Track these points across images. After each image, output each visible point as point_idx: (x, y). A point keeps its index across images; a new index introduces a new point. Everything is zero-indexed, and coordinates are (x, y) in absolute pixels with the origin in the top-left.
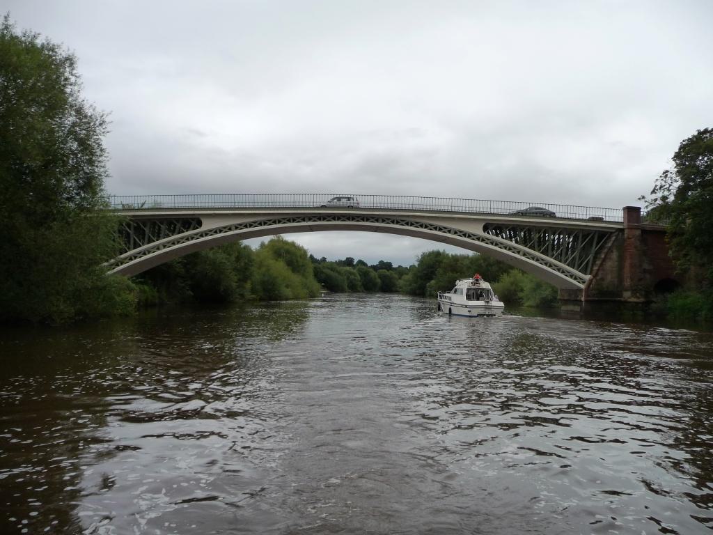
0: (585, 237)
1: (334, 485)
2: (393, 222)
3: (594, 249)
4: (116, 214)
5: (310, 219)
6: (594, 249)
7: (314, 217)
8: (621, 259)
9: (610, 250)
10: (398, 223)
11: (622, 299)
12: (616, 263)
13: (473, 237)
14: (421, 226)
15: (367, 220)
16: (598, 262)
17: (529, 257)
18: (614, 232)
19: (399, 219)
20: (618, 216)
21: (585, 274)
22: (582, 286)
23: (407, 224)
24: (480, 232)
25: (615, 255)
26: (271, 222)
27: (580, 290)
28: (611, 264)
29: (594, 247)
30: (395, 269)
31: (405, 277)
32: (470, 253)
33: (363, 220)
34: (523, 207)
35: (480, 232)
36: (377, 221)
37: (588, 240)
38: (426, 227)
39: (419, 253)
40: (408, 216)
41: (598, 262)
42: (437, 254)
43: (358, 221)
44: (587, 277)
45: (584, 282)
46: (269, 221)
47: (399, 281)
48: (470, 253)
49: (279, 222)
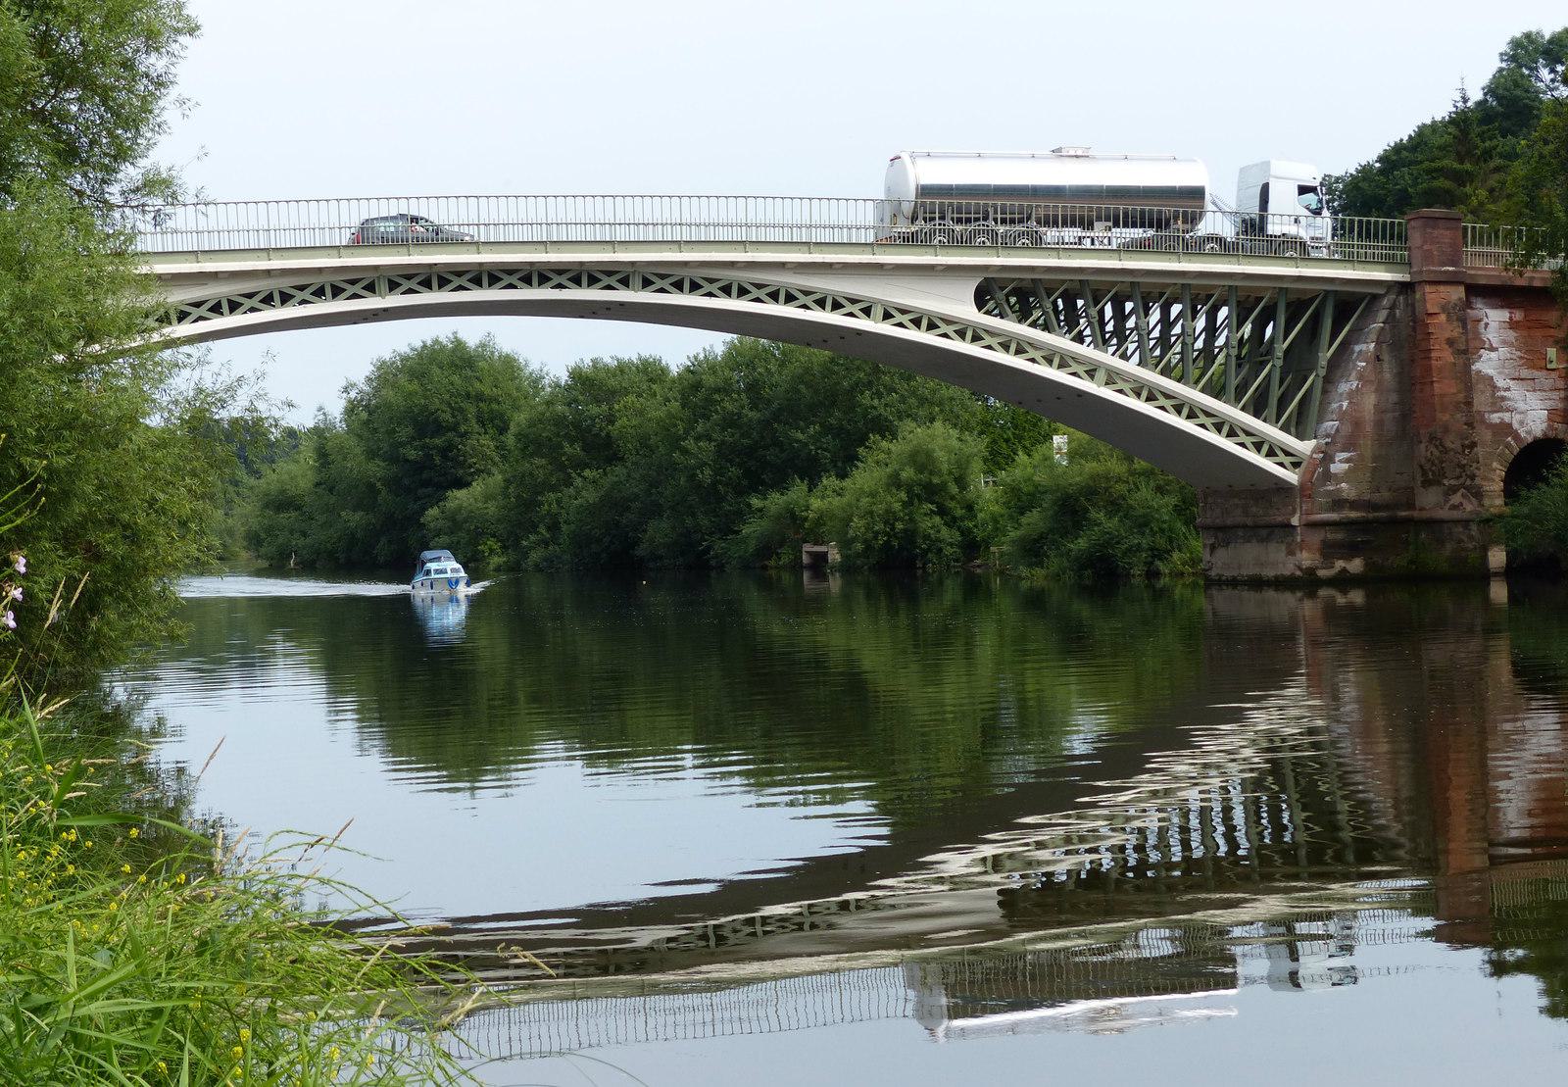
0: (1296, 309)
1: (1527, 68)
2: (679, 286)
5: (393, 286)
7: (409, 277)
10: (695, 287)
11: (1416, 514)
12: (1394, 397)
13: (849, 308)
14: (774, 296)
15: (593, 281)
17: (1126, 387)
18: (1384, 296)
19: (698, 274)
21: (1300, 436)
23: (727, 291)
26: (254, 302)
29: (1277, 387)
32: (716, 343)
33: (577, 281)
35: (966, 310)
36: (625, 282)
38: (790, 298)
39: (360, 372)
40: (732, 265)
43: (560, 286)
44: (1305, 447)
45: (1296, 465)
46: (250, 296)
48: (679, 348)
49: (285, 299)
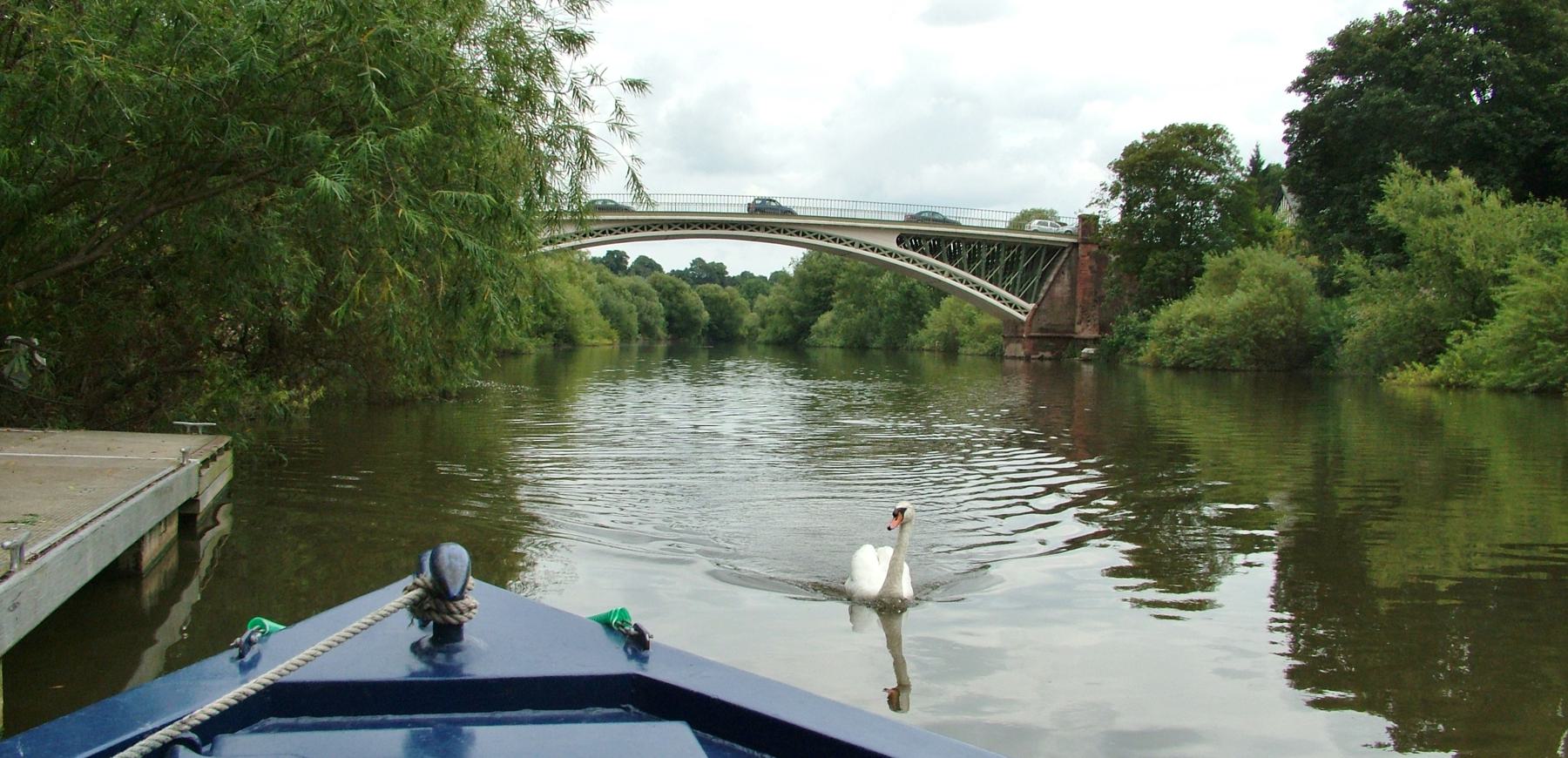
0: (1009, 249)
3: (1040, 270)
4: (634, 251)
6: (1040, 270)
8: (1073, 284)
9: (1061, 272)
16: (1045, 287)
20: (1073, 223)
22: (1024, 318)
24: (894, 246)
25: (1066, 279)
27: (1022, 322)
28: (1061, 289)
30: (734, 281)
31: (762, 301)
34: (914, 211)
35: (894, 246)
37: (1014, 256)
41: (1045, 287)
42: (609, 253)
44: (1030, 306)
47: (460, 49)
